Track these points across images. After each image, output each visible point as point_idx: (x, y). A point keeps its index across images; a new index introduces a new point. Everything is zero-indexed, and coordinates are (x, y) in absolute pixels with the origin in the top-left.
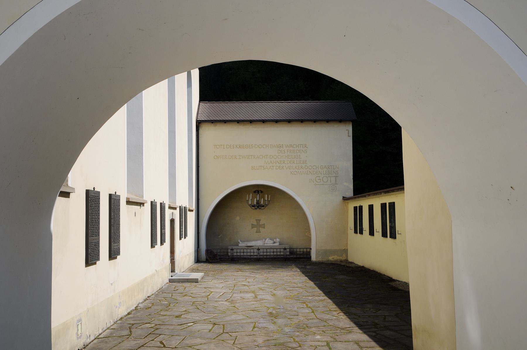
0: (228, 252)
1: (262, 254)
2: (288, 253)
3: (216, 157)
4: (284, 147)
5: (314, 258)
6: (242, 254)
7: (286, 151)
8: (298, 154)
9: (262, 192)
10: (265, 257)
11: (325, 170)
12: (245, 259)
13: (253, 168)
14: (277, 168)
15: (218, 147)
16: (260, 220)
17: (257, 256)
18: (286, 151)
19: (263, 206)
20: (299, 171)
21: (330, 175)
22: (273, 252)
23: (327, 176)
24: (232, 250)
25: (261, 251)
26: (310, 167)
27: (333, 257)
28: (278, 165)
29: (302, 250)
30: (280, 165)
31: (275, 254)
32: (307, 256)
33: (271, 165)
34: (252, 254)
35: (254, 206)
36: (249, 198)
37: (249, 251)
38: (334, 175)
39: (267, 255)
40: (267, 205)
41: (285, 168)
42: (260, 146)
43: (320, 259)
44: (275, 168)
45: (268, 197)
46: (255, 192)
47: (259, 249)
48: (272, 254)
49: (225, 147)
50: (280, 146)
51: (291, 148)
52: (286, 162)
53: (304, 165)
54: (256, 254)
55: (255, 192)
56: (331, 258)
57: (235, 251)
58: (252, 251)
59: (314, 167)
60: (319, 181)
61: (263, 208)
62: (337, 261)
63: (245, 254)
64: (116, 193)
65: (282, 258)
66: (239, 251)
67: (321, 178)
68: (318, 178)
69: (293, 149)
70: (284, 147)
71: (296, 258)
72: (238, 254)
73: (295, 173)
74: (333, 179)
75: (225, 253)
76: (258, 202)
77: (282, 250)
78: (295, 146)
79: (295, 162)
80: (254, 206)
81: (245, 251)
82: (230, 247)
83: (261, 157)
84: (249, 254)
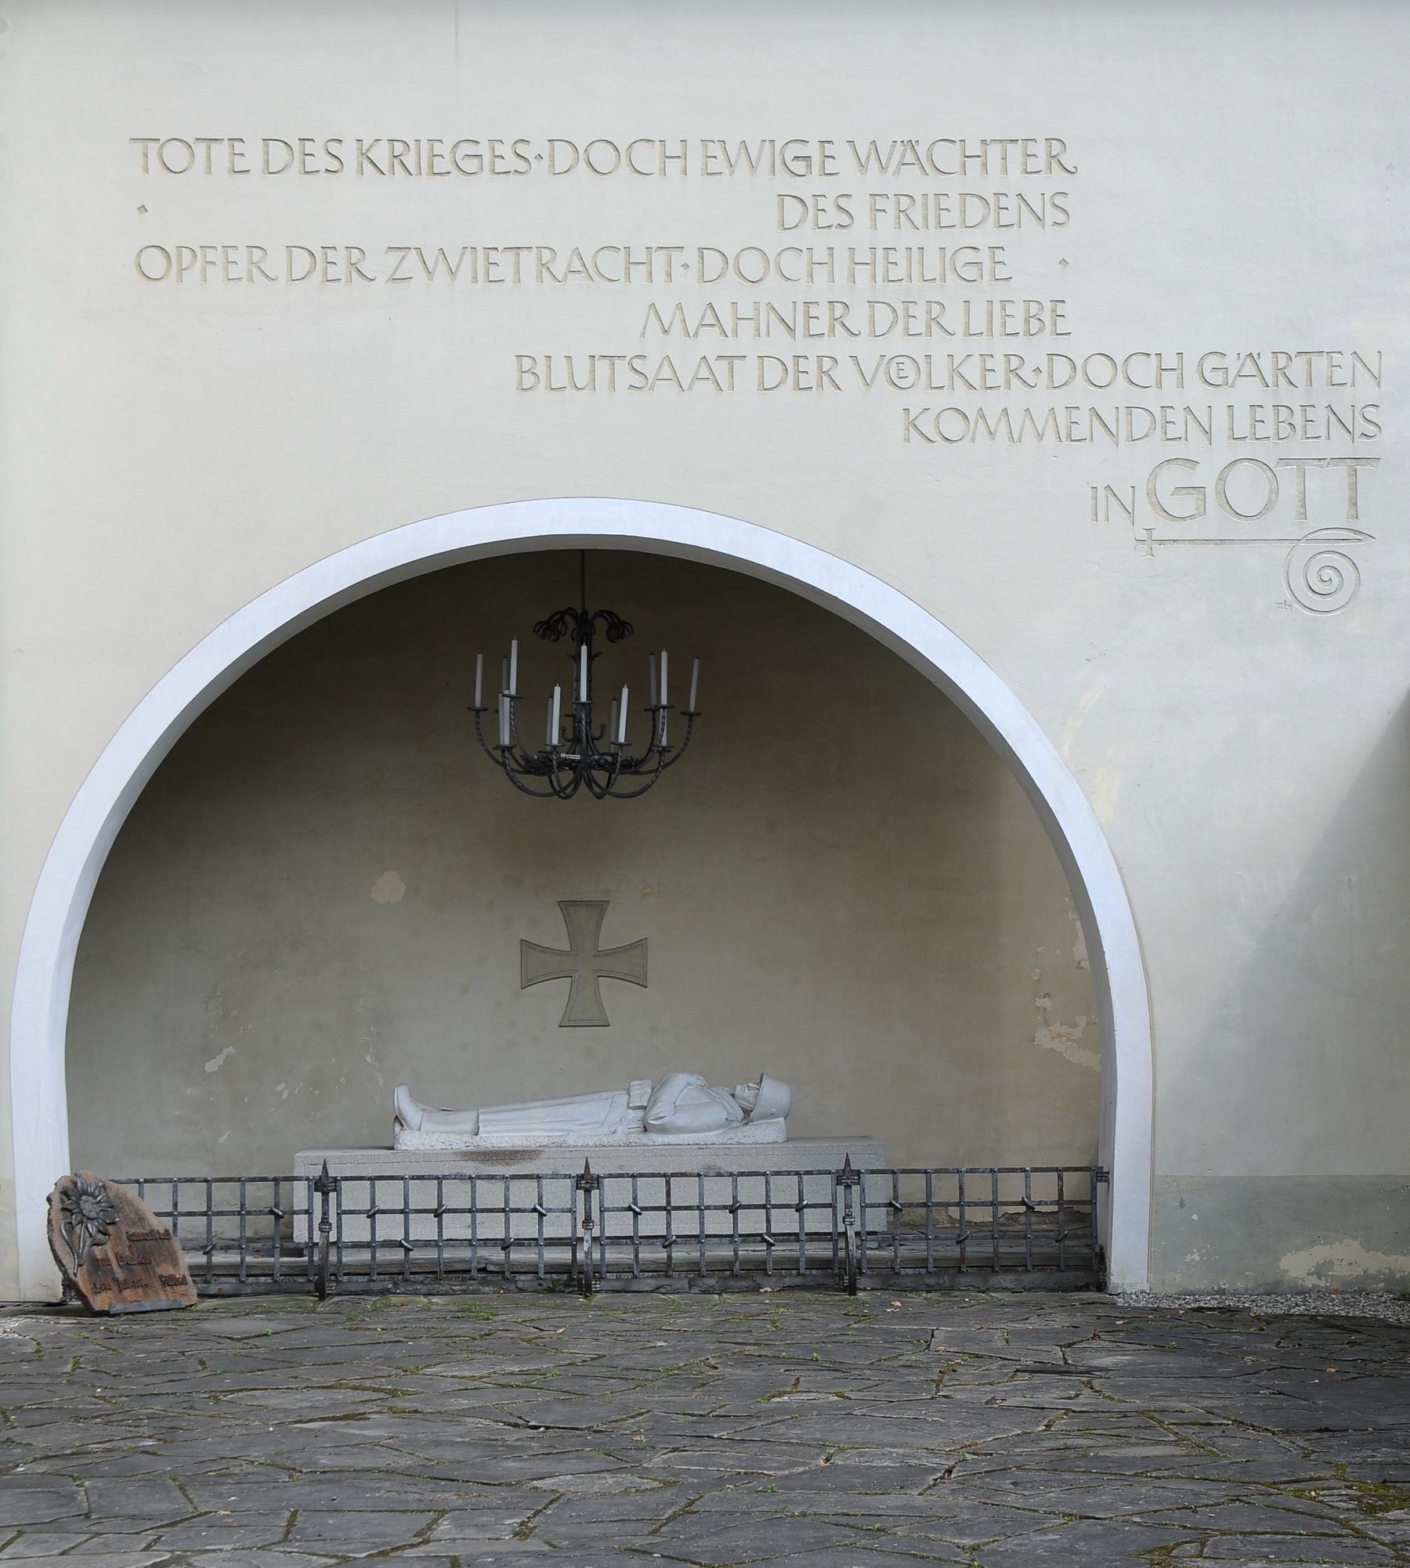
0: (281, 1216)
1: (619, 1225)
2: (878, 1220)
3: (154, 263)
4: (844, 163)
5: (1130, 1264)
6: (423, 1229)
7: (860, 208)
8: (986, 237)
9: (618, 629)
10: (653, 1254)
11: (1248, 391)
12: (461, 1272)
13: (529, 372)
14: (773, 374)
15: (176, 155)
16: (599, 907)
17: (573, 1243)
18: (862, 214)
19: (631, 767)
20: (993, 403)
21: (1296, 448)
22: (242, 1212)
23: (1265, 452)
24: (324, 1185)
25: (616, 1193)
26: (1100, 371)
27: (1321, 1253)
28: (781, 345)
29: (1012, 1188)
30: (802, 345)
31: (752, 1222)
32: (1065, 1250)
33: (710, 343)
34: (524, 1227)
35: (542, 765)
36: (494, 686)
37: (490, 1194)
38: (1338, 445)
39: (666, 1242)
40: (666, 758)
41: (845, 373)
42: (602, 157)
43: (1193, 1277)
44: (747, 372)
45: (678, 688)
46: (550, 628)
47: (587, 1182)
48: (719, 1223)
49: (253, 158)
50: (800, 159)
51: (912, 181)
52: (857, 319)
53: (1035, 352)
54: (558, 1227)
55: (550, 628)
56: (1297, 1265)
57: (355, 1196)
58: (524, 1195)
59: (1144, 372)
60: (1186, 505)
61: (625, 783)
62: (1359, 1289)
63: (456, 1228)
64: (587, 1167)
65: (815, 1263)
66: (389, 1195)
67: (1205, 476)
68: (1175, 476)
69: (931, 184)
70: (844, 163)
71: (957, 1267)
72: (389, 1228)
73: (952, 426)
74: (1326, 490)
75: (266, 1224)
76: (584, 725)
77: (819, 1189)
78: (947, 157)
79: (953, 319)
80: (542, 765)
81: (457, 1195)
82: (306, 1164)
83: (612, 265)
84: (491, 1227)
